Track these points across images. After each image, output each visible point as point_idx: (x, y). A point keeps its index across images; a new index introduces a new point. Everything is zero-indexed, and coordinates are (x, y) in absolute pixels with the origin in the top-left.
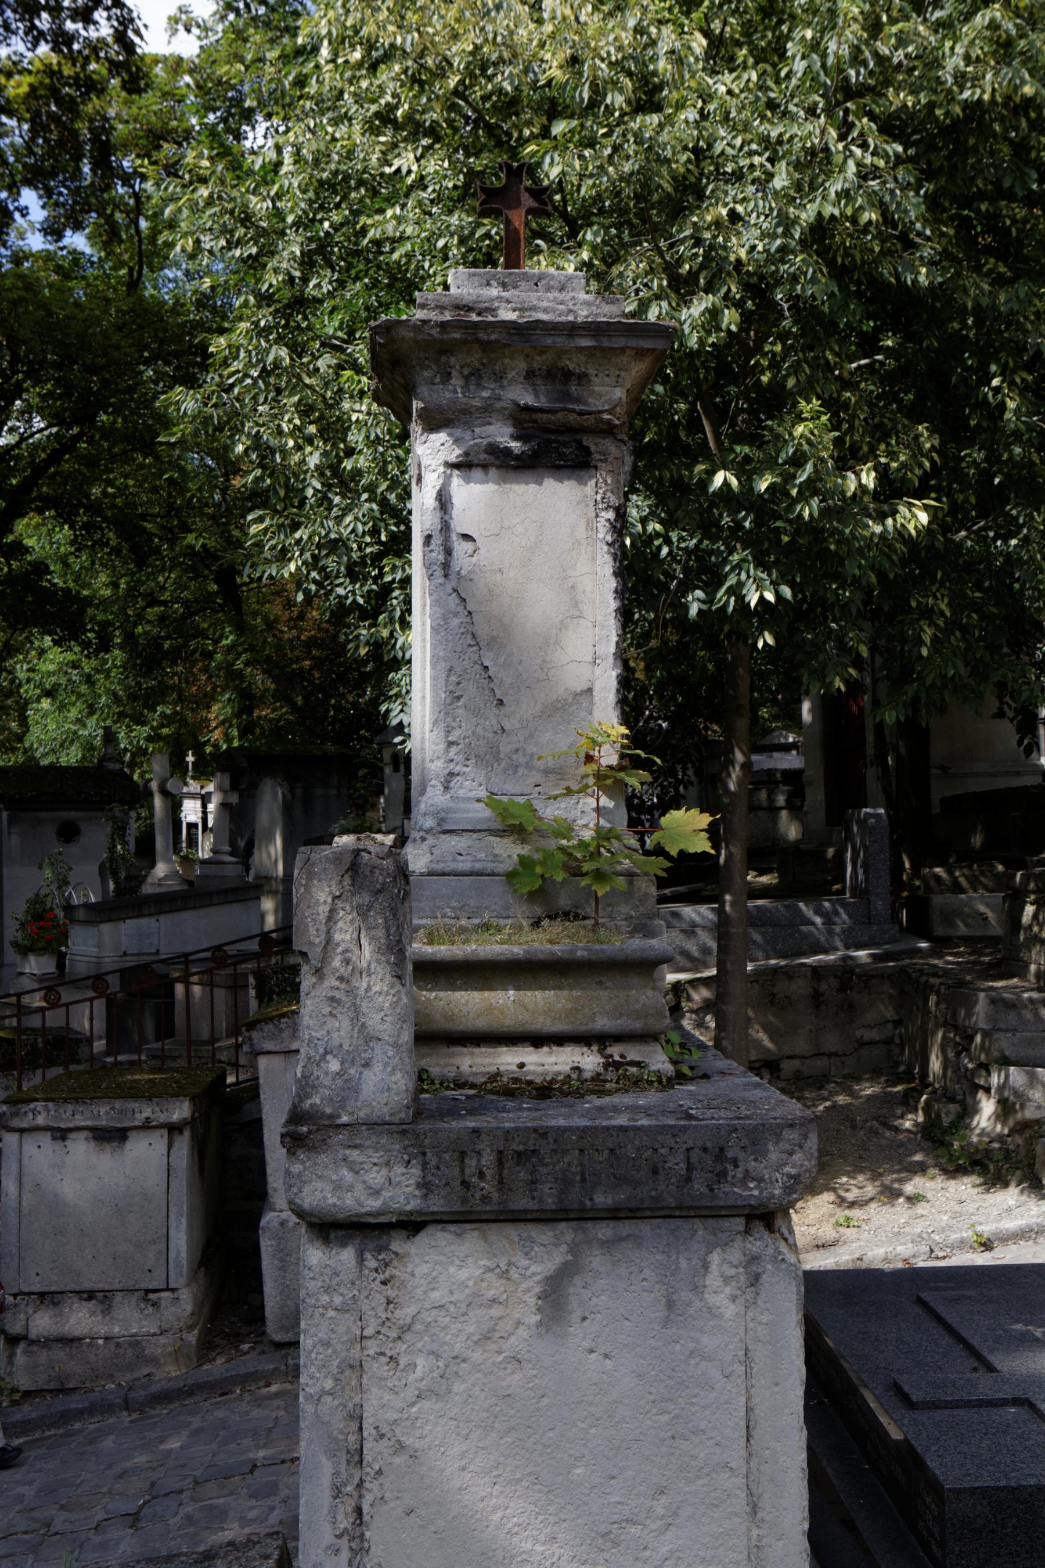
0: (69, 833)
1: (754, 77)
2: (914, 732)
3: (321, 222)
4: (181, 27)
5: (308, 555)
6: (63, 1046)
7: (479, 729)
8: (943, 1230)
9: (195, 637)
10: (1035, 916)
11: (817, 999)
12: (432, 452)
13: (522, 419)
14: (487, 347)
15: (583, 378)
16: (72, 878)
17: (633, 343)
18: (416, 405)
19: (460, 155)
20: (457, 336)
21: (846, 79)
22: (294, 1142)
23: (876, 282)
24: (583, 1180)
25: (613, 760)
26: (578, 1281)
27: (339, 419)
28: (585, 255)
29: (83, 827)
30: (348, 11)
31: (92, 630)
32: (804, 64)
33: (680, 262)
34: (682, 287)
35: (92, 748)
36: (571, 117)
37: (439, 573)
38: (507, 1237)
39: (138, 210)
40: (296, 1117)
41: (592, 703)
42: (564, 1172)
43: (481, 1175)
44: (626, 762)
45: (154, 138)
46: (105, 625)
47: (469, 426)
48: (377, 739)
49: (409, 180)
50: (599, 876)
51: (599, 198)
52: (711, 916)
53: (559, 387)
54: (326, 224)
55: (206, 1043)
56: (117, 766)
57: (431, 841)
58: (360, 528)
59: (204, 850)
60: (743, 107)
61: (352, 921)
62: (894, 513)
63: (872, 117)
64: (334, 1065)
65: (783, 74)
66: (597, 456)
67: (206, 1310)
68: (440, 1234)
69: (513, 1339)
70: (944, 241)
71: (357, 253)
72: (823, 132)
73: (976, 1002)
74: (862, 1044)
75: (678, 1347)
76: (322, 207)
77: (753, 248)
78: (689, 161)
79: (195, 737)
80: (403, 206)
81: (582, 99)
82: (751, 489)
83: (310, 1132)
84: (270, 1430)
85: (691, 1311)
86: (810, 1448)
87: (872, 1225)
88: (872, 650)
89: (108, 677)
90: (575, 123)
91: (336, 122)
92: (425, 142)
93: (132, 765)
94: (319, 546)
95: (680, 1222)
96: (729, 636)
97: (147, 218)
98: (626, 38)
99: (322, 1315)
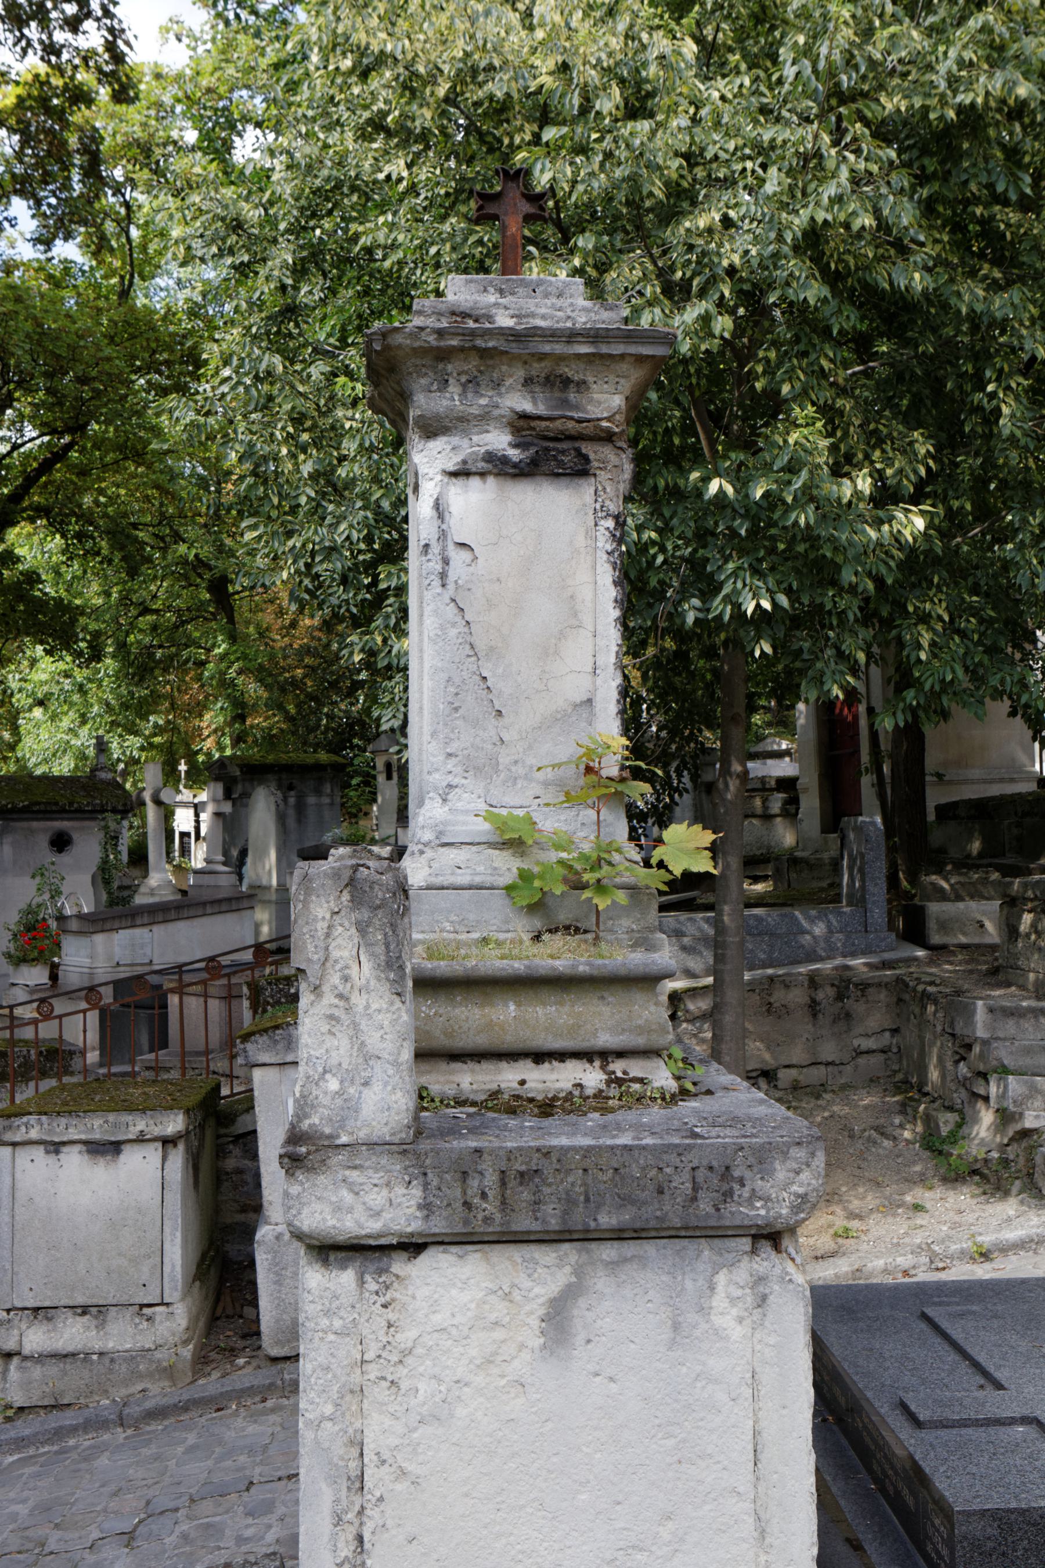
0: (61, 843)
1: (747, 82)
2: (911, 737)
3: (313, 229)
4: (171, 36)
5: (301, 564)
6: (56, 1058)
8: (943, 1241)
9: (187, 646)
10: (1034, 925)
11: (814, 1008)
12: (429, 459)
13: (521, 424)
14: (484, 354)
15: (582, 386)
16: (65, 889)
17: (633, 349)
18: (412, 413)
19: (452, 164)
21: (838, 84)
22: (293, 1162)
23: (871, 290)
24: (587, 1200)
25: (614, 772)
26: (582, 1303)
27: (333, 428)
28: (577, 262)
29: (75, 836)
30: (338, 19)
31: (84, 640)
32: (795, 69)
33: (672, 269)
34: (677, 293)
35: (84, 757)
36: (564, 123)
37: (437, 583)
38: (509, 1259)
39: (129, 218)
40: (295, 1137)
41: (592, 714)
42: (567, 1193)
43: (484, 1196)
44: (626, 774)
45: (142, 151)
46: (97, 635)
47: (466, 433)
48: (370, 748)
49: (401, 187)
50: (600, 887)
51: (590, 205)
53: (557, 394)
54: (318, 232)
55: (198, 1054)
56: (110, 776)
57: (429, 853)
59: (198, 858)
60: (736, 113)
61: (350, 937)
62: (891, 519)
63: (867, 123)
64: (333, 1085)
65: (774, 78)
67: (201, 1324)
68: (441, 1256)
69: (516, 1363)
70: (938, 247)
71: (349, 261)
72: (816, 136)
73: (974, 1011)
74: (859, 1053)
75: (684, 1370)
76: (314, 215)
77: (746, 252)
78: (681, 167)
79: (188, 745)
80: (395, 213)
81: (572, 106)
82: (747, 496)
83: (309, 1153)
84: (266, 1447)
85: (697, 1333)
86: (818, 1470)
87: (870, 1236)
88: (869, 656)
89: (100, 686)
90: (565, 130)
91: (328, 128)
92: (416, 148)
93: (125, 773)
95: (685, 1242)
96: (726, 643)
97: (138, 227)
98: (616, 43)
99: (322, 1339)
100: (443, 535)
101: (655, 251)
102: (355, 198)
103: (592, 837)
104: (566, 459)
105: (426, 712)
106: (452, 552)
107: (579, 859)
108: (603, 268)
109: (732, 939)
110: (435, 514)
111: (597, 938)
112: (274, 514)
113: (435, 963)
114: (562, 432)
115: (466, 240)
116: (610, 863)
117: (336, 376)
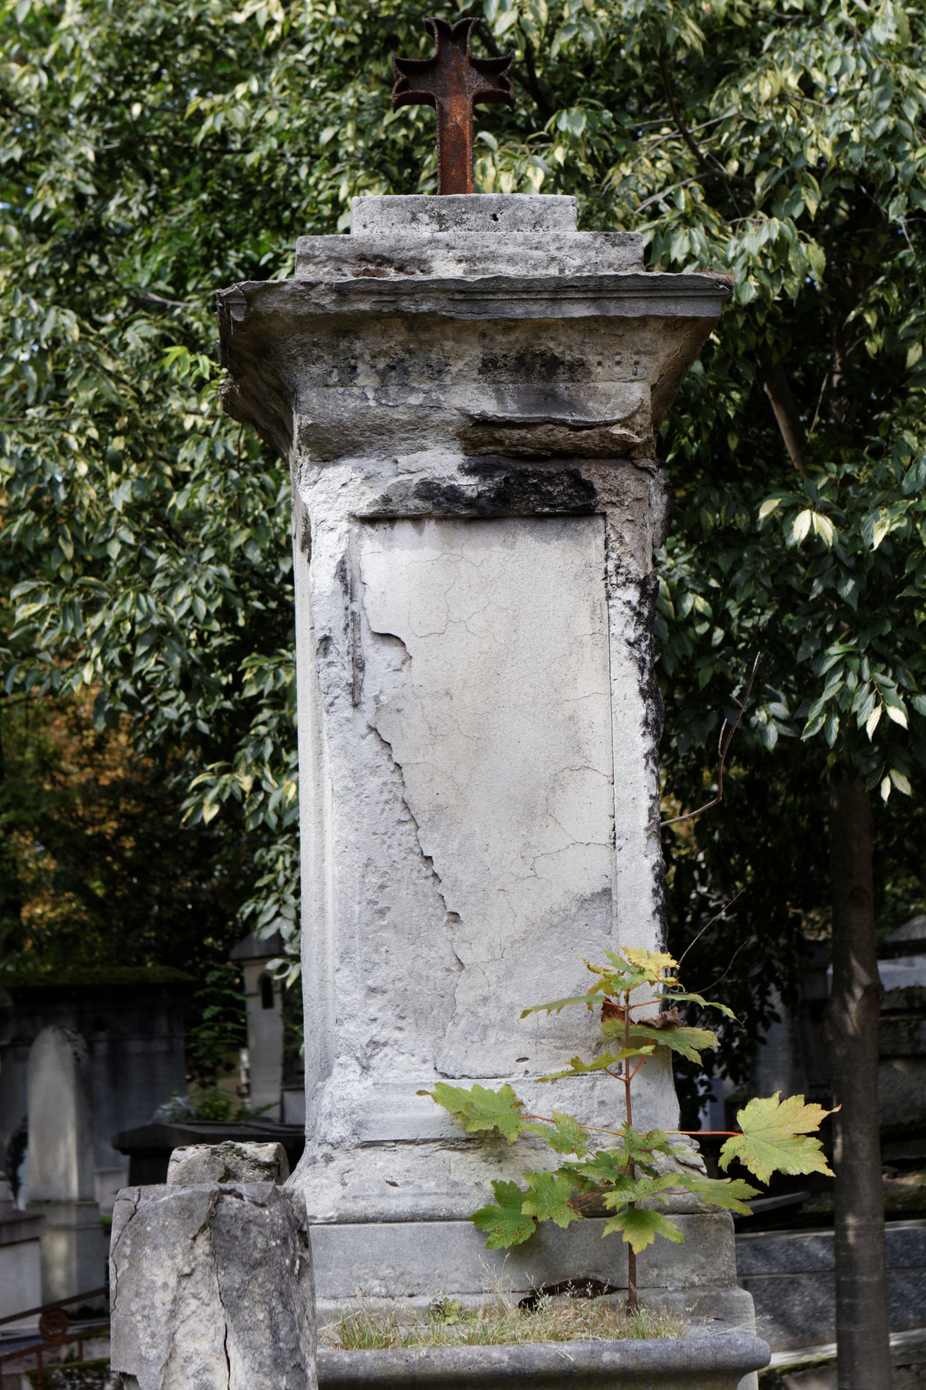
3: (128, 104)
7: (420, 962)
12: (326, 498)
13: (477, 436)
14: (416, 323)
15: (578, 370)
17: (660, 309)
18: (299, 421)
20: (365, 306)
25: (652, 1012)
27: (164, 428)
33: (724, 156)
34: (729, 200)
37: (345, 700)
41: (612, 914)
47: (387, 452)
49: (272, 36)
50: (635, 1215)
52: (823, 1253)
53: (538, 385)
54: (136, 109)
57: (342, 1161)
58: (202, 608)
66: (605, 497)
71: (189, 153)
76: (129, 81)
77: (844, 137)
82: (857, 538)
94: (133, 638)
100: (353, 621)
101: (695, 129)
102: (195, 54)
103: (618, 1125)
104: (555, 490)
105: (330, 917)
106: (371, 650)
107: (596, 1165)
108: (605, 163)
109: (866, 1278)
110: (338, 586)
111: (632, 1302)
112: (66, 574)
113: (357, 1354)
114: (547, 446)
115: (381, 116)
116: (649, 1170)
117: (170, 344)
